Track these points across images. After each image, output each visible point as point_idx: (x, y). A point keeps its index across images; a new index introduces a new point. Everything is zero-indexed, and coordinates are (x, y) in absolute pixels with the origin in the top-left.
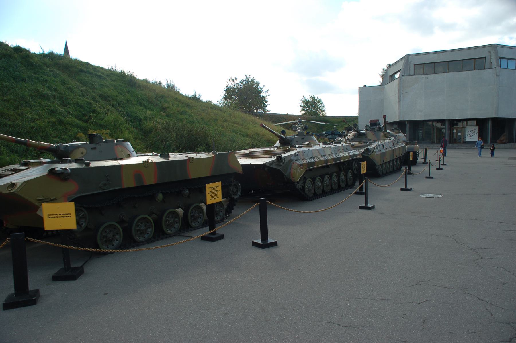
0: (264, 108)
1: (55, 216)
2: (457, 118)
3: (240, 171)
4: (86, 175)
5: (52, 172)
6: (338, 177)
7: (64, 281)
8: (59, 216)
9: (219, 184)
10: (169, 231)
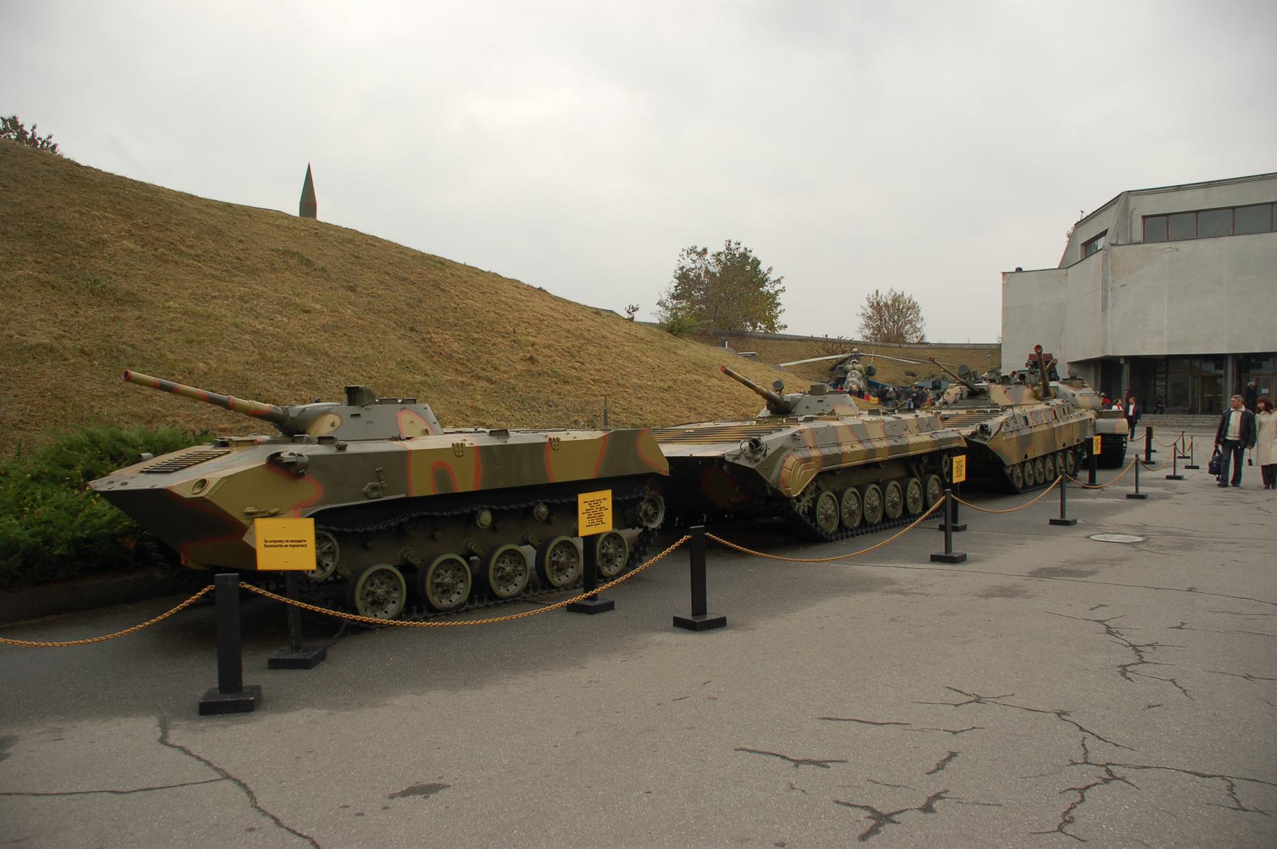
0: (770, 322)
1: (277, 544)
2: (1257, 349)
3: (665, 469)
4: (339, 467)
5: (274, 460)
6: (903, 492)
9: (607, 494)
10: (502, 591)
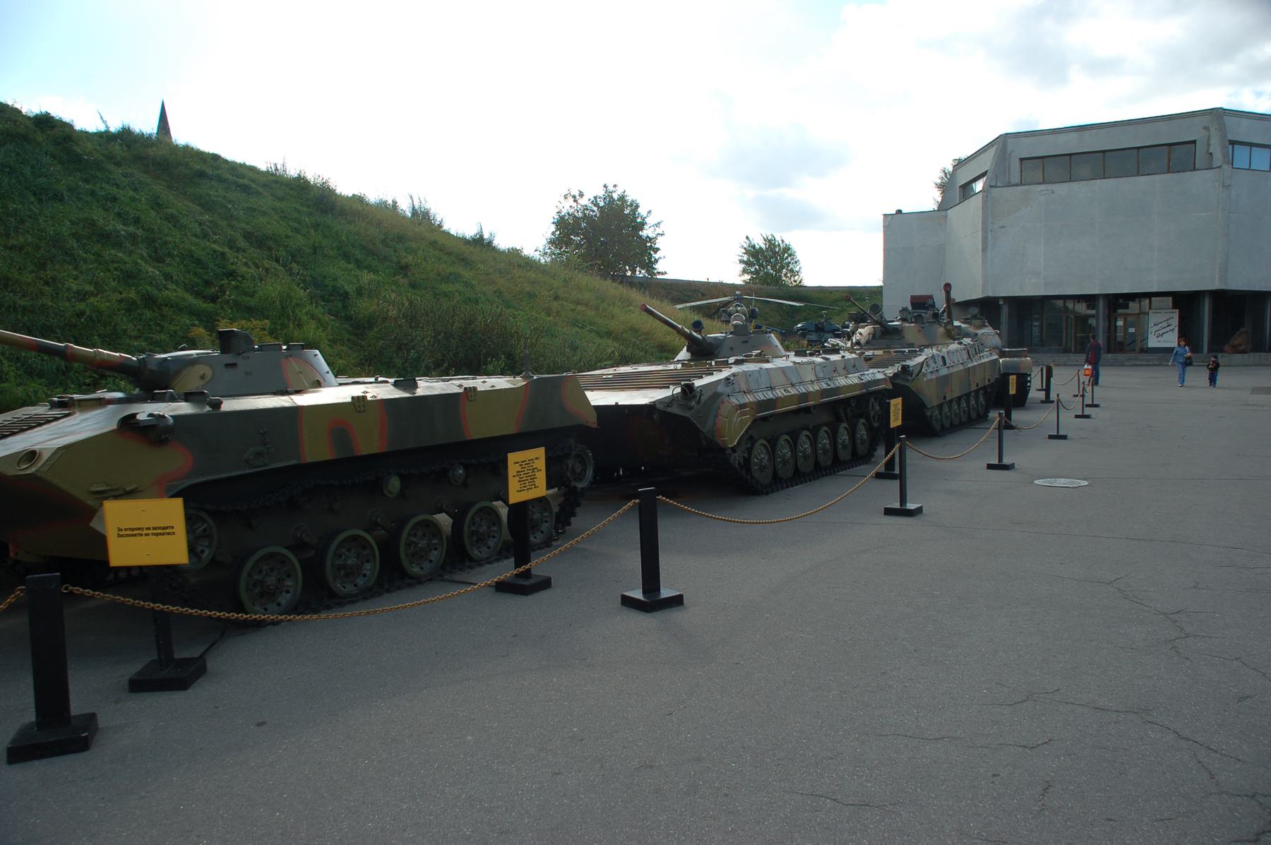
0: (649, 265)
1: (135, 532)
2: (1126, 290)
3: (592, 420)
4: (211, 430)
5: (129, 423)
6: (833, 436)
8: (145, 532)
9: (540, 453)
10: (416, 570)
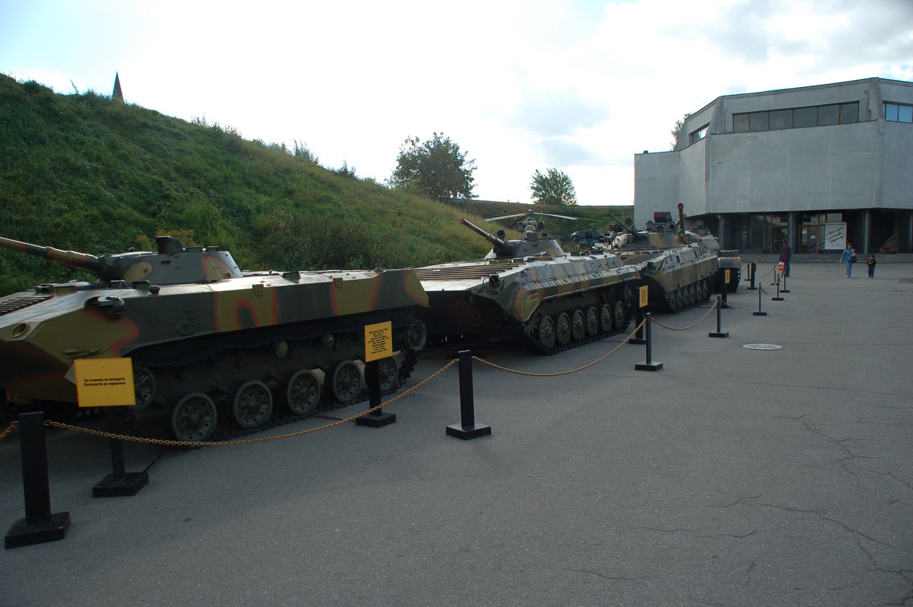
0: (467, 191)
1: (97, 382)
2: (809, 208)
3: (425, 302)
4: (151, 309)
5: (92, 304)
6: (599, 313)
7: (113, 498)
8: (104, 382)
9: (388, 325)
10: (299, 409)
